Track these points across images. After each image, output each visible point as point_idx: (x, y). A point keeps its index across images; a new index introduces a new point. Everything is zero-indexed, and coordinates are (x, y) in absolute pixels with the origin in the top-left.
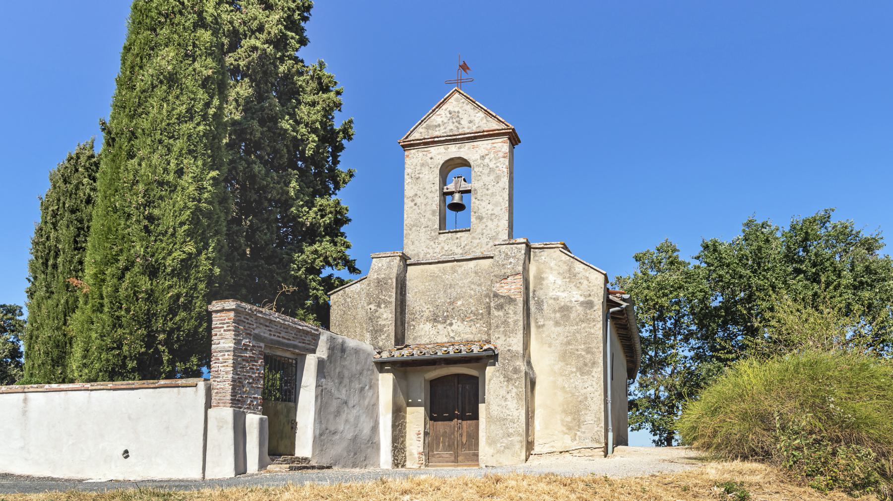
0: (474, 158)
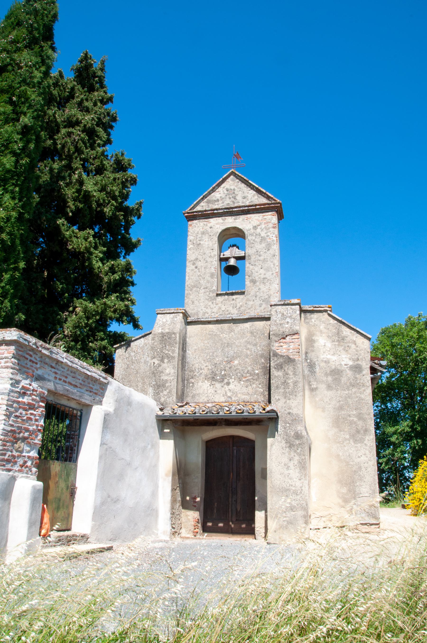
0: (247, 228)
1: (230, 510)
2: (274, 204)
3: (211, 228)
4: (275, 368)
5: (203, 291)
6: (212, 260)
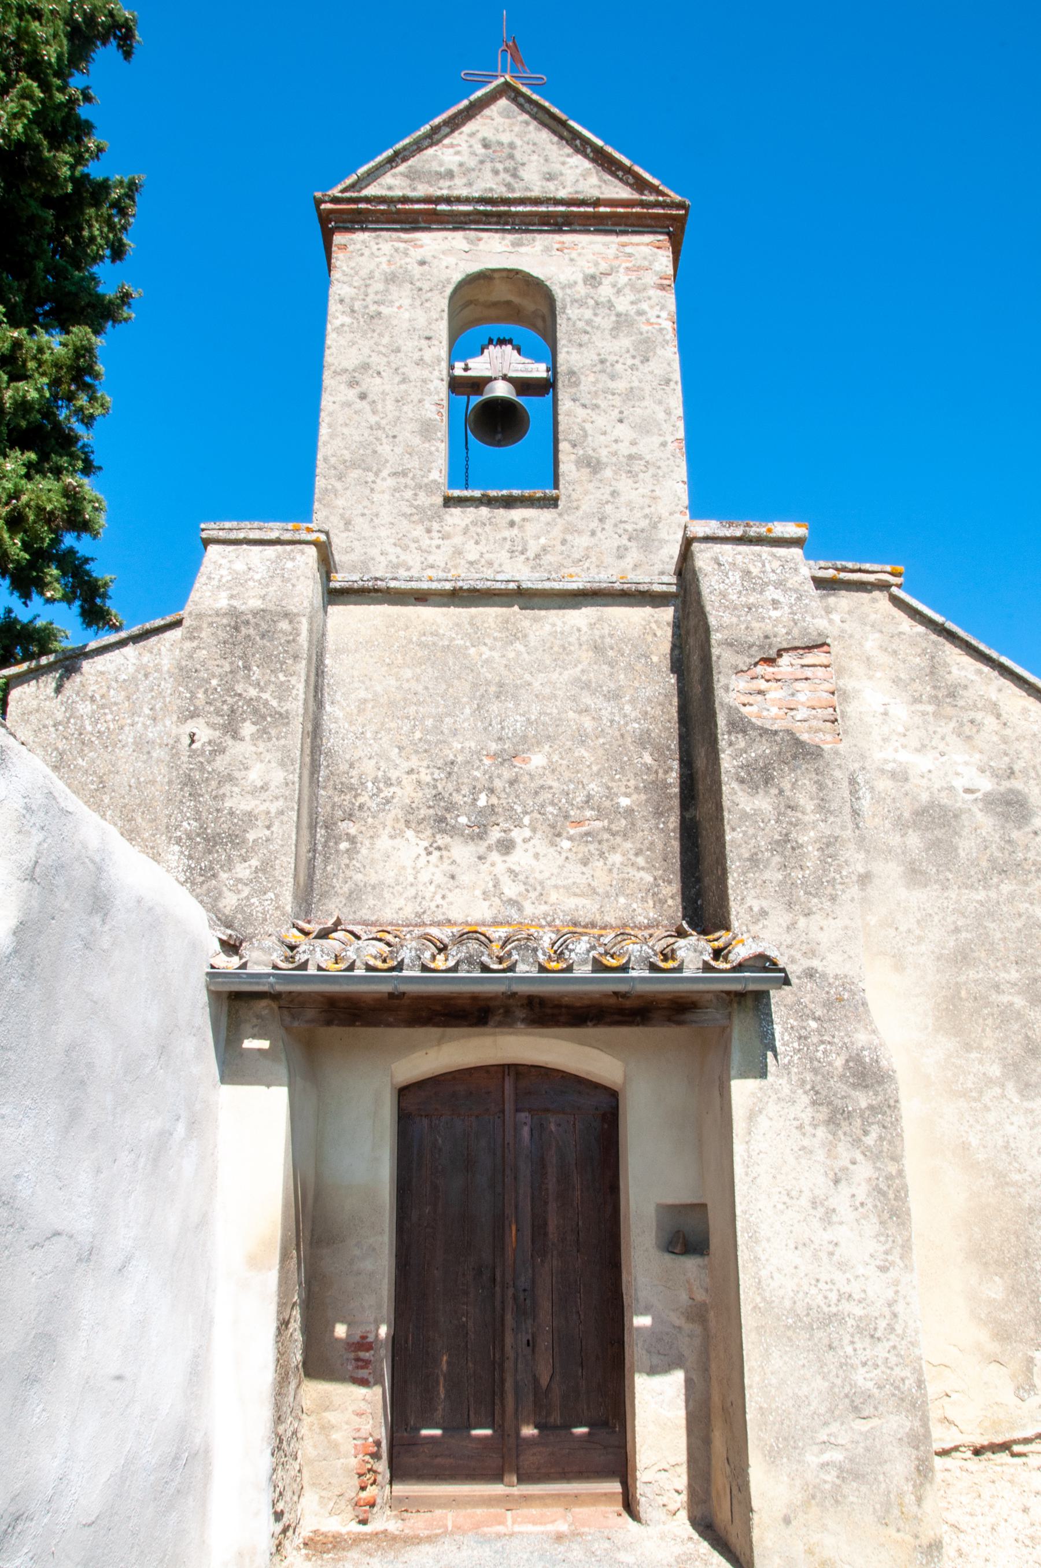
0: (563, 278)
1: (509, 1385)
2: (657, 204)
3: (422, 263)
4: (742, 781)
5: (391, 482)
6: (426, 373)
